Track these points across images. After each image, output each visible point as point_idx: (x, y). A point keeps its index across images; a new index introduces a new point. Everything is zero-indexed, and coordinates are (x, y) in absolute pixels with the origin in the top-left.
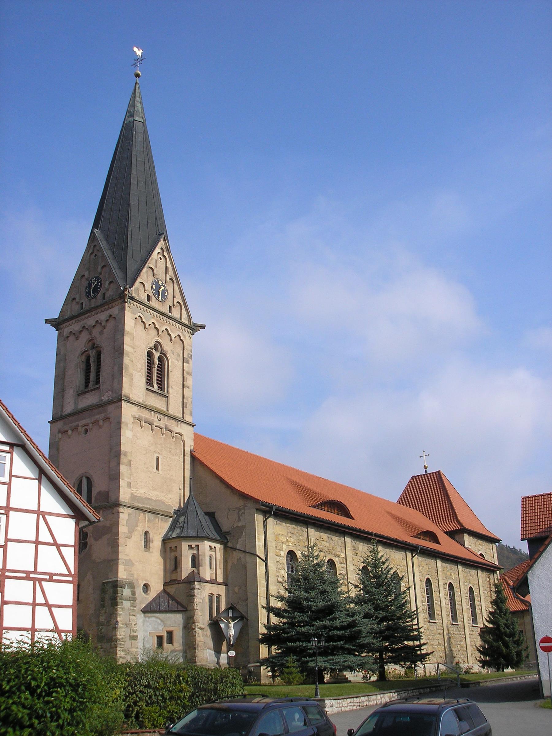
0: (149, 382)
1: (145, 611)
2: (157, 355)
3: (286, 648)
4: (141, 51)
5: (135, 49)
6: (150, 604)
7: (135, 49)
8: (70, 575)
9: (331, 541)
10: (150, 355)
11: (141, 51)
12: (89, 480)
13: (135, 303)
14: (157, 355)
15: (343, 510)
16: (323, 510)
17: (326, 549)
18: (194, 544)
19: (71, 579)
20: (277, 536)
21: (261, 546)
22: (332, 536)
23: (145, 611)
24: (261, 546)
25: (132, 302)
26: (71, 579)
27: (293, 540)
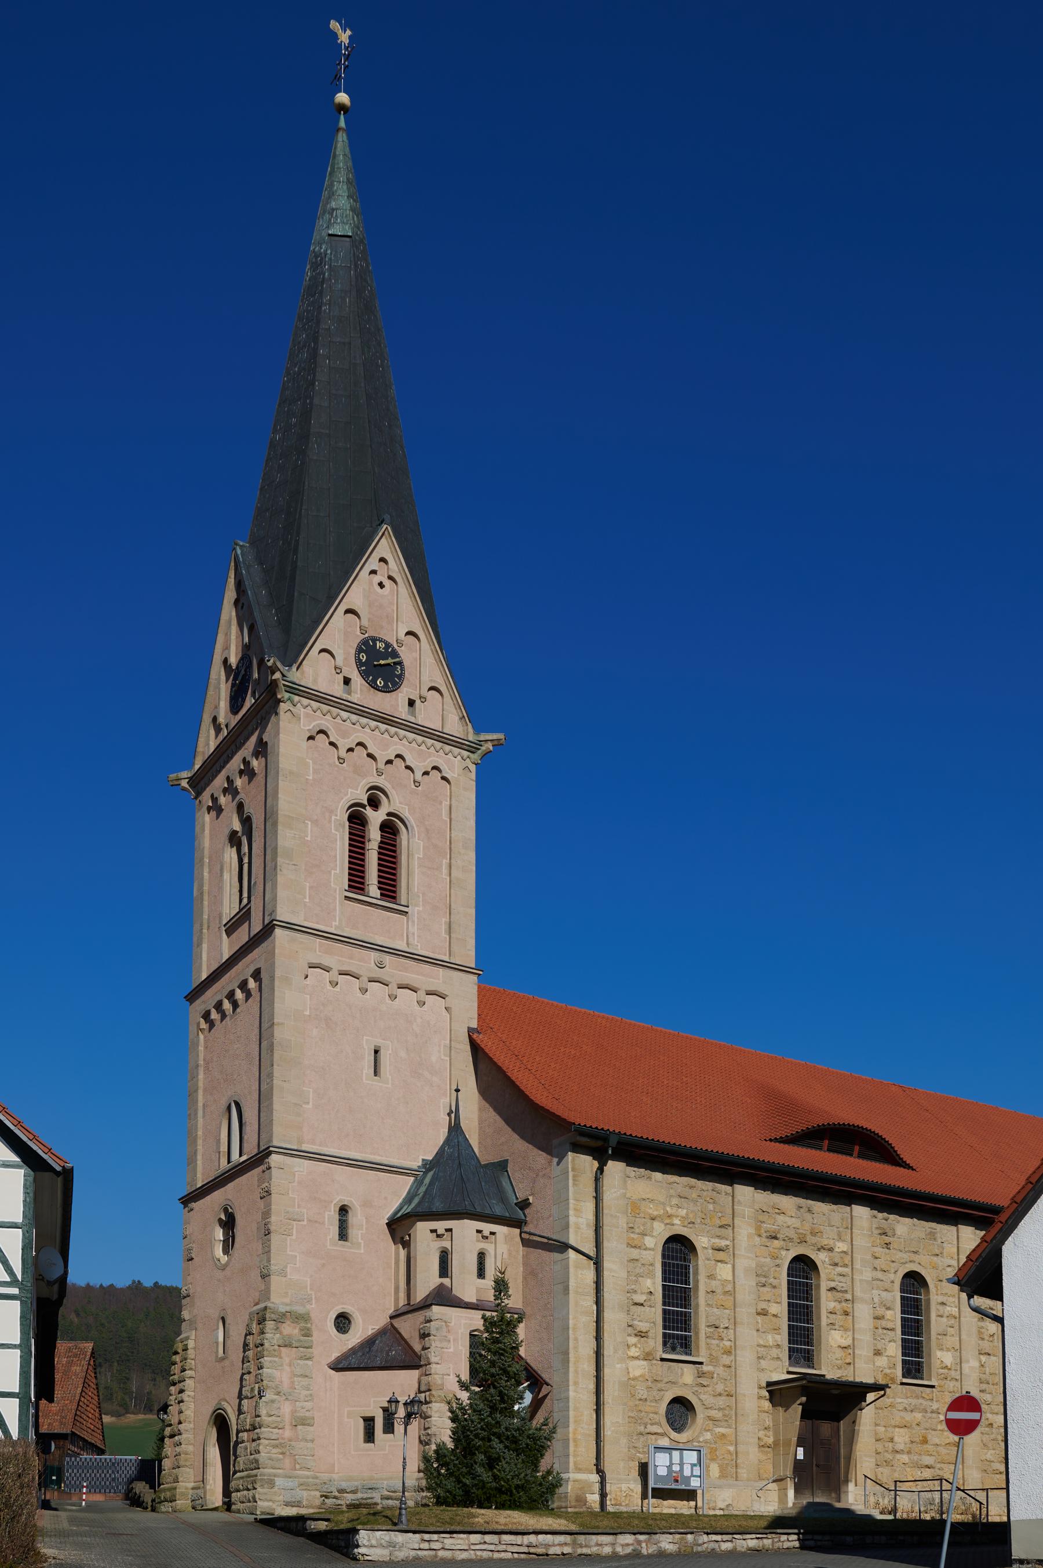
0: (356, 881)
1: (339, 1366)
2: (375, 818)
3: (798, 1445)
4: (349, 32)
5: (334, 25)
6: (353, 1351)
7: (334, 25)
8: (14, 1282)
9: (808, 1216)
10: (357, 819)
11: (349, 32)
12: (237, 1104)
13: (306, 702)
14: (375, 818)
15: (877, 1148)
16: (820, 1148)
17: (792, 1234)
18: (441, 1226)
19: (15, 1291)
20: (634, 1208)
21: (583, 1226)
22: (810, 1202)
23: (339, 1366)
24: (583, 1226)
25: (296, 698)
26: (15, 1291)
27: (683, 1212)
